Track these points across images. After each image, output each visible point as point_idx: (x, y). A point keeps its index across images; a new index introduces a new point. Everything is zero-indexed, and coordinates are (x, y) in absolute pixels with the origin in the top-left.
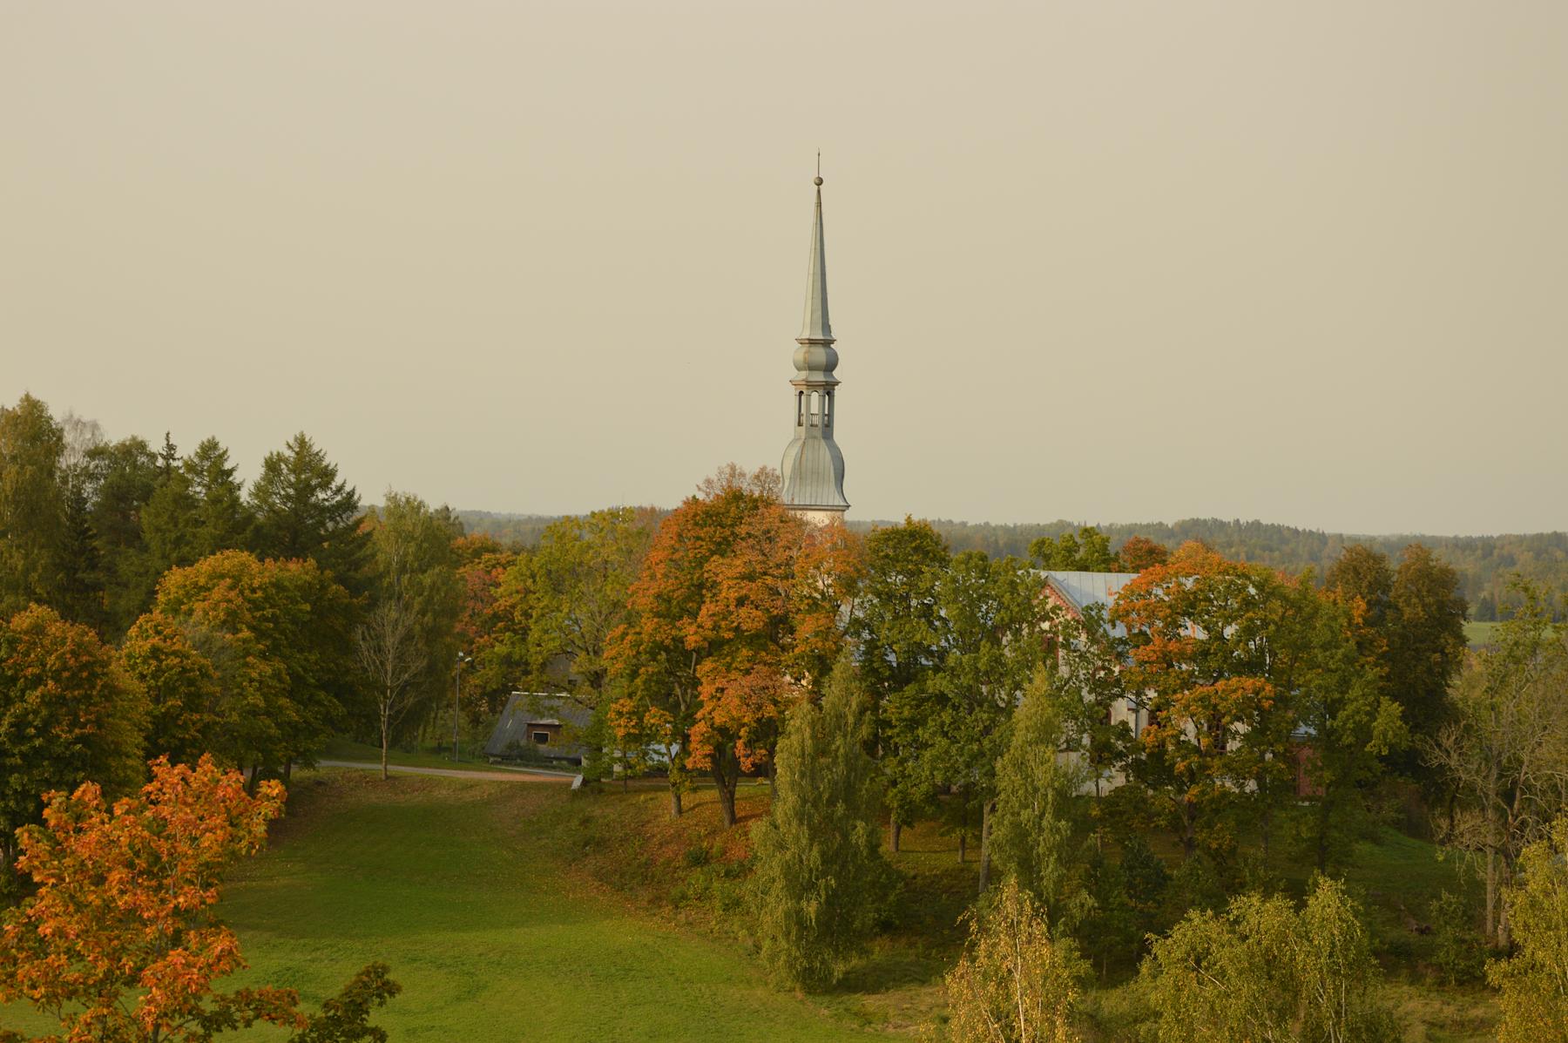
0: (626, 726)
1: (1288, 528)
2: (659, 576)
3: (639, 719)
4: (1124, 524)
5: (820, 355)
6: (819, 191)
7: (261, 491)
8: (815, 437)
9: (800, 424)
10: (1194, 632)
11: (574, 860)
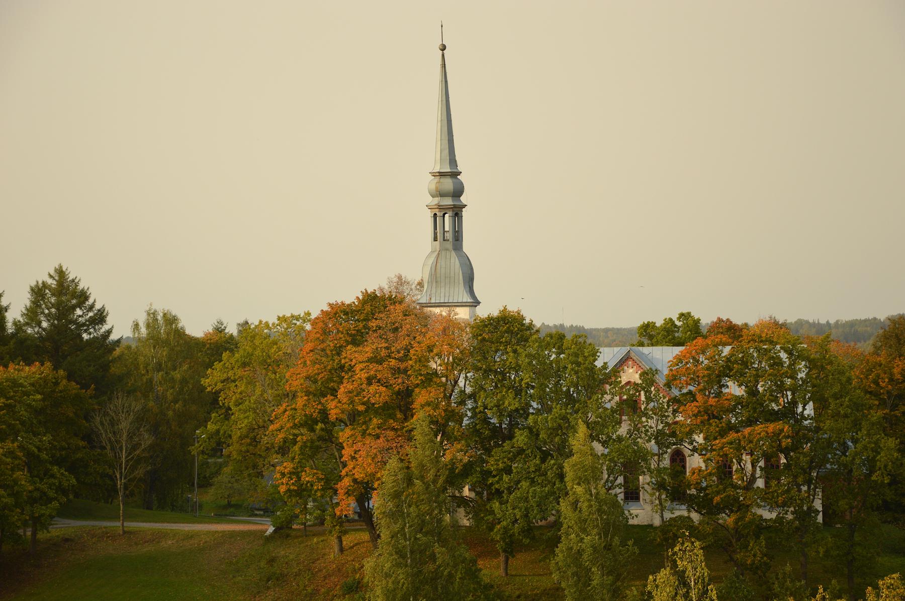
2: (308, 363)
6: (443, 55)
7: (32, 314)
8: (447, 250)
9: (435, 239)
10: (734, 389)
11: (259, 592)
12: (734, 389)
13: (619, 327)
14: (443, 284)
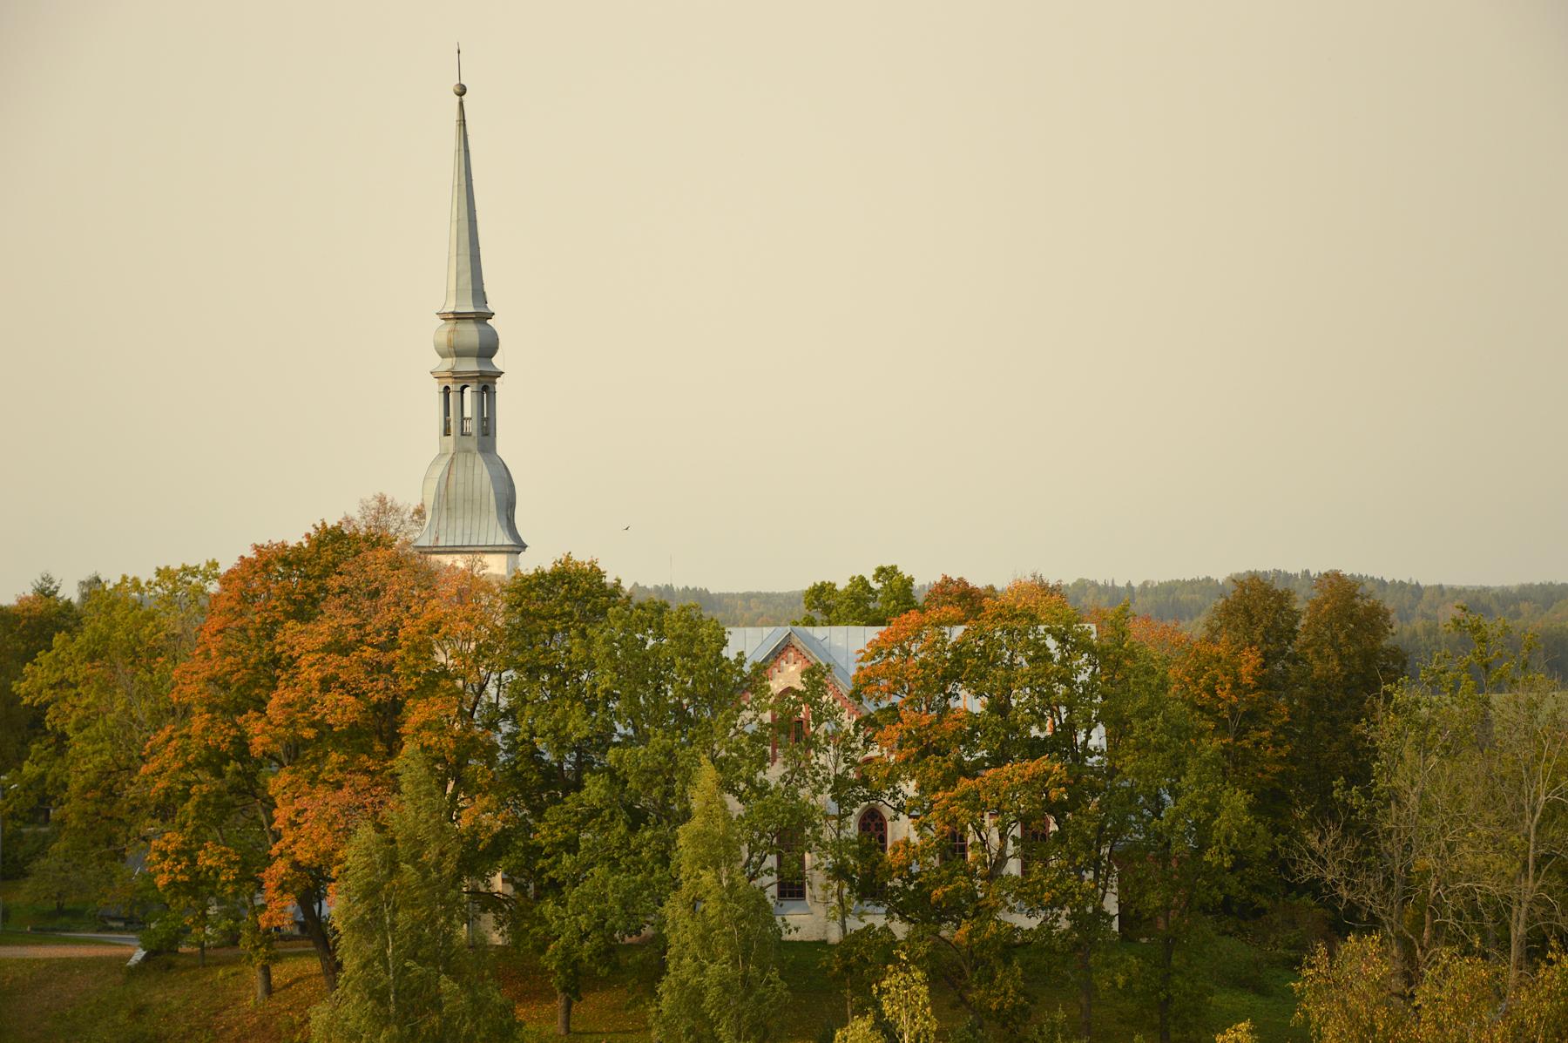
0: (171, 871)
1: (1372, 579)
3: (190, 860)
4: (1162, 581)
5: (470, 334)
6: (461, 104)
8: (468, 451)
9: (447, 432)
10: (969, 702)
12: (969, 702)
13: (770, 591)
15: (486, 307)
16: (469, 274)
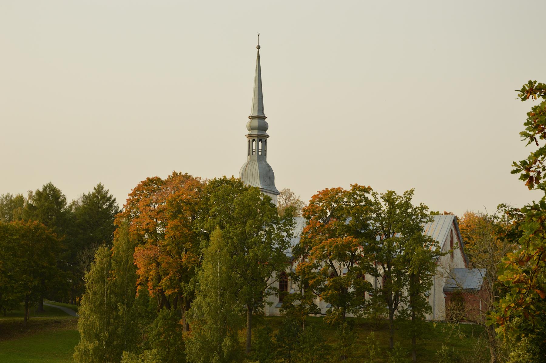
5: (256, 122)
6: (258, 51)
9: (249, 155)
14: (249, 179)
15: (263, 113)
16: (257, 104)
